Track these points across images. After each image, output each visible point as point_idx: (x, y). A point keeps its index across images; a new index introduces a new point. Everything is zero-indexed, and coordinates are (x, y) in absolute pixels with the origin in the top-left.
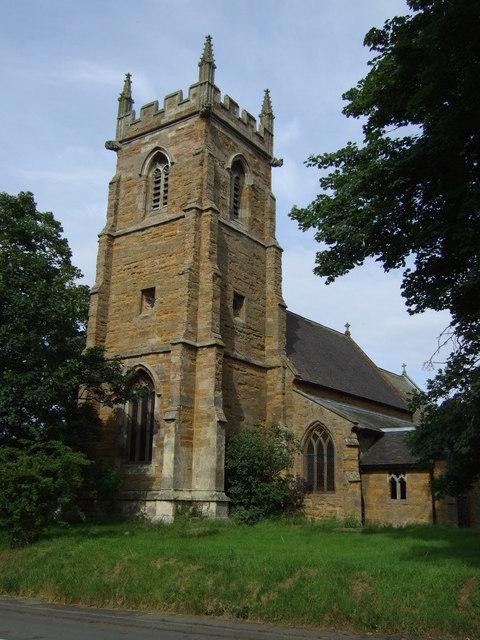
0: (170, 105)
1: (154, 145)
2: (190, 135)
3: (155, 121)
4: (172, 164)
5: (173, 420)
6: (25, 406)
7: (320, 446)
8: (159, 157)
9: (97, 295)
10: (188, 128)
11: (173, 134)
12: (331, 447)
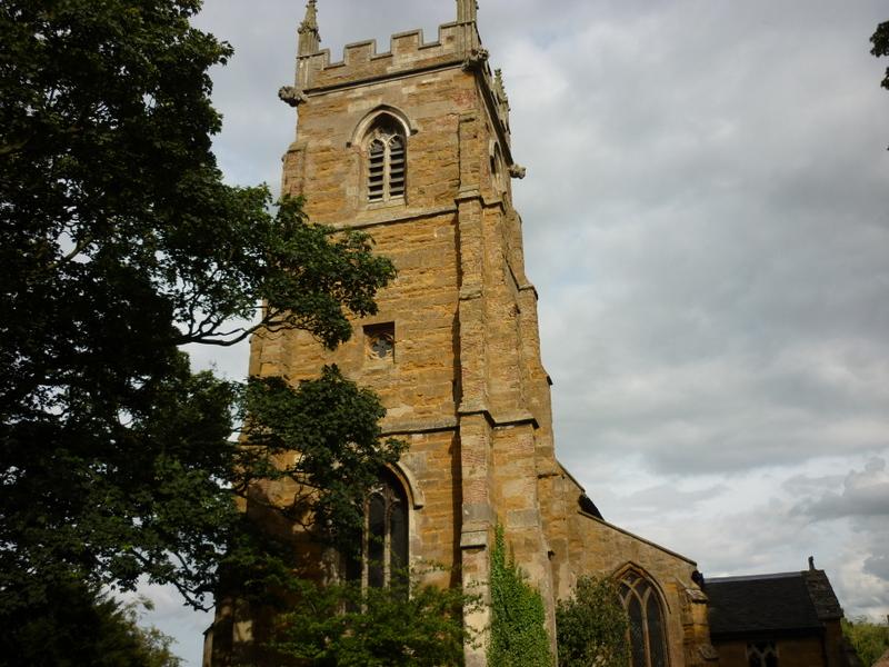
0: (403, 49)
1: (379, 102)
2: (445, 92)
3: (366, 69)
4: (414, 132)
5: (482, 547)
6: (100, 564)
7: (634, 602)
8: (385, 122)
9: (427, 41)
10: (441, 82)
11: (413, 89)
12: (656, 602)
